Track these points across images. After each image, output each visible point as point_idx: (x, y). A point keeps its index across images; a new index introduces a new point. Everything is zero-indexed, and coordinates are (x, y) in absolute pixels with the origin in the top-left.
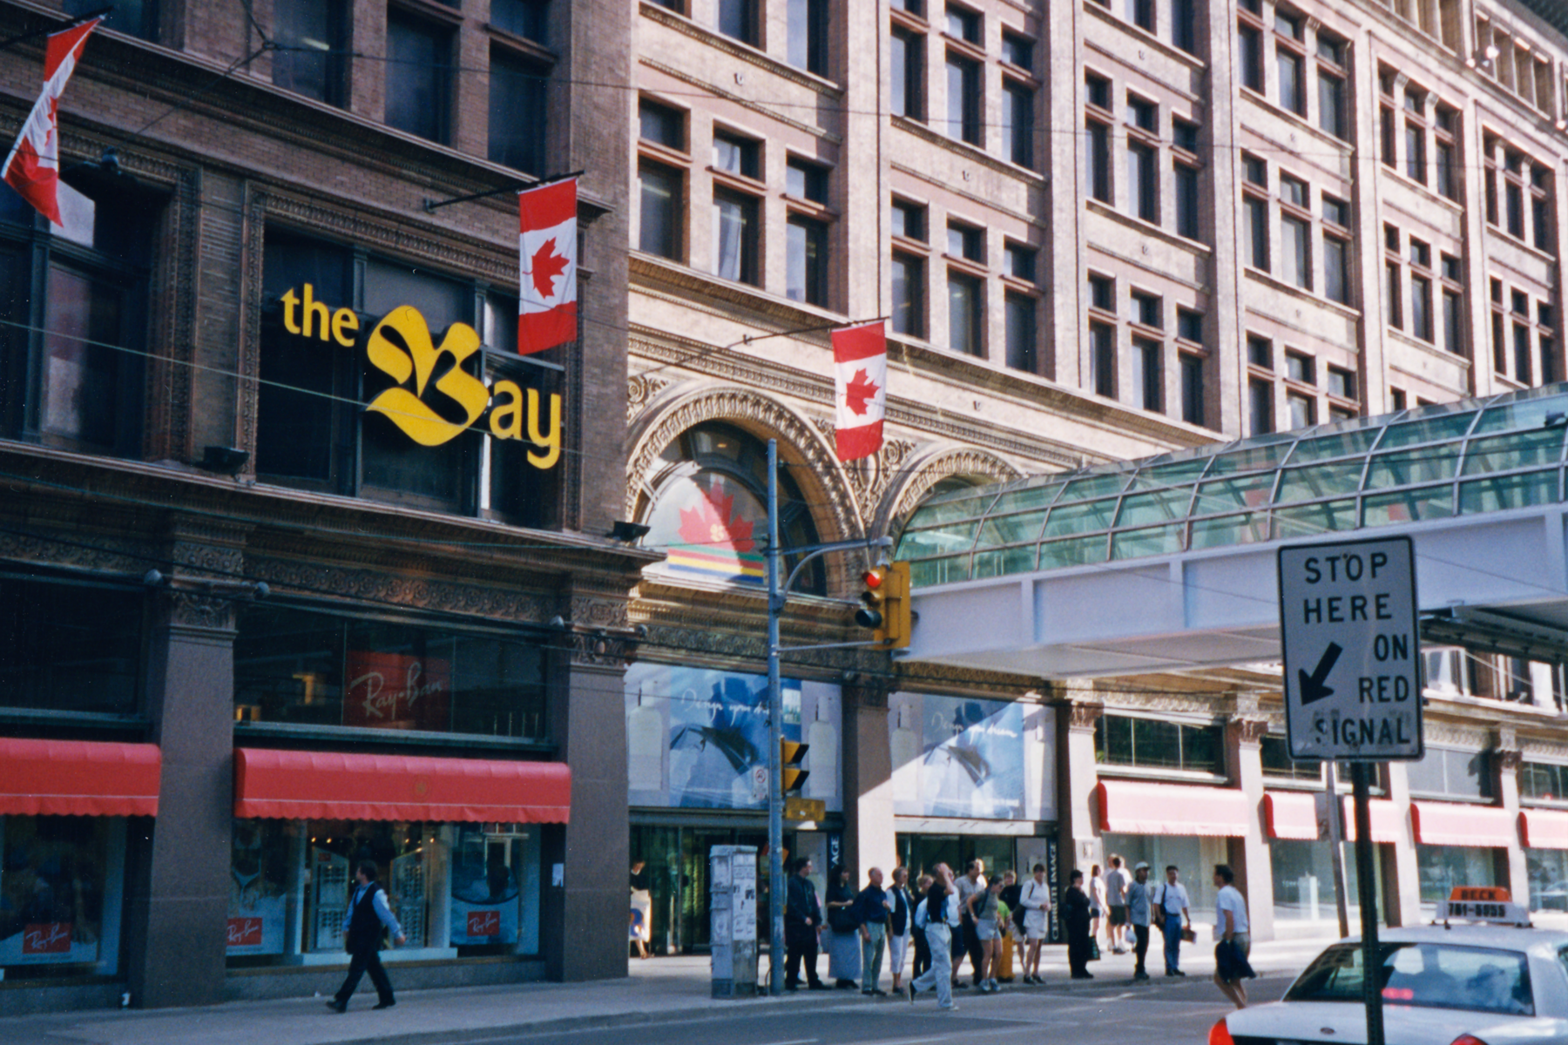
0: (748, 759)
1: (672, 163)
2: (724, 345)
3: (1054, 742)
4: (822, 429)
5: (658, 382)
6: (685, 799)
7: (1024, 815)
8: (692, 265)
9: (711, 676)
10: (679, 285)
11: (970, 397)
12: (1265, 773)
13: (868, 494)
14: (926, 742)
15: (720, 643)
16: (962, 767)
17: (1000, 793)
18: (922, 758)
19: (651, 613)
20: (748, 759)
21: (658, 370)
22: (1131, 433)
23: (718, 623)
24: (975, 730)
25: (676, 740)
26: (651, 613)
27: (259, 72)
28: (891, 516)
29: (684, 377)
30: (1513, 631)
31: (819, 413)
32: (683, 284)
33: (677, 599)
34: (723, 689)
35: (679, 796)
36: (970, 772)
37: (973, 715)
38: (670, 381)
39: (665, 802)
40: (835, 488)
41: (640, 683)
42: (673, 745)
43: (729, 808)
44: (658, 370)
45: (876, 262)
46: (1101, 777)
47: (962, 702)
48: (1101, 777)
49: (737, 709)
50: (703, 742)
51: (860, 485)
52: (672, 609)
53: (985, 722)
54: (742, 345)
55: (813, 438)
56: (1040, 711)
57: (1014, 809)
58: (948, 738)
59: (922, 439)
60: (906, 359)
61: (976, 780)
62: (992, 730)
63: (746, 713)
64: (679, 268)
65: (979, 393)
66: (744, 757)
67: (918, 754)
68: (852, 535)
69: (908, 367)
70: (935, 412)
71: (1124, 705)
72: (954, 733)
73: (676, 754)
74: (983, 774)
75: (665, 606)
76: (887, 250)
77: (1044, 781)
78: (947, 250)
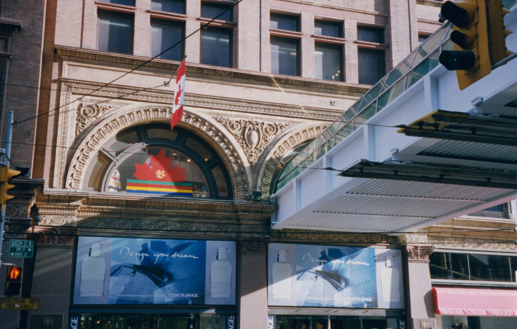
0: (166, 280)
1: (370, 47)
2: (108, 82)
3: (401, 269)
4: (220, 122)
5: (283, 124)
6: (119, 300)
7: (377, 306)
8: (134, 54)
9: (140, 241)
10: (117, 62)
11: (327, 100)
12: (432, 277)
13: (253, 150)
14: (298, 268)
15: (150, 225)
16: (326, 281)
17: (356, 294)
18: (296, 277)
19: (100, 212)
20: (166, 280)
21: (106, 101)
22: (264, 87)
23: (147, 215)
24: (335, 263)
25: (115, 272)
26: (100, 212)
27: (5, 17)
28: (268, 158)
29: (124, 104)
30: (493, 170)
31: (218, 114)
32: (118, 61)
33: (116, 205)
34: (327, 253)
35: (116, 298)
36: (333, 284)
37: (338, 255)
38: (115, 106)
39: (106, 302)
40: (228, 148)
41: (91, 245)
42: (112, 275)
43: (152, 304)
44: (106, 101)
45: (259, 42)
46: (434, 285)
47: (326, 248)
48: (434, 285)
49: (158, 256)
50: (316, 277)
51: (247, 146)
52: (113, 210)
53: (344, 258)
54: (164, 86)
55: (211, 125)
56: (388, 251)
57: (368, 303)
58: (316, 266)
59: (292, 122)
60: (277, 85)
61: (337, 287)
62: (352, 262)
63: (165, 257)
64: (129, 57)
65: (333, 97)
66: (340, 283)
67: (293, 275)
68: (240, 170)
69: (280, 88)
70: (300, 108)
71: (460, 247)
72: (320, 264)
73: (114, 279)
74: (343, 284)
75: (108, 209)
76: (266, 36)
77: (392, 288)
78: (149, 8)
